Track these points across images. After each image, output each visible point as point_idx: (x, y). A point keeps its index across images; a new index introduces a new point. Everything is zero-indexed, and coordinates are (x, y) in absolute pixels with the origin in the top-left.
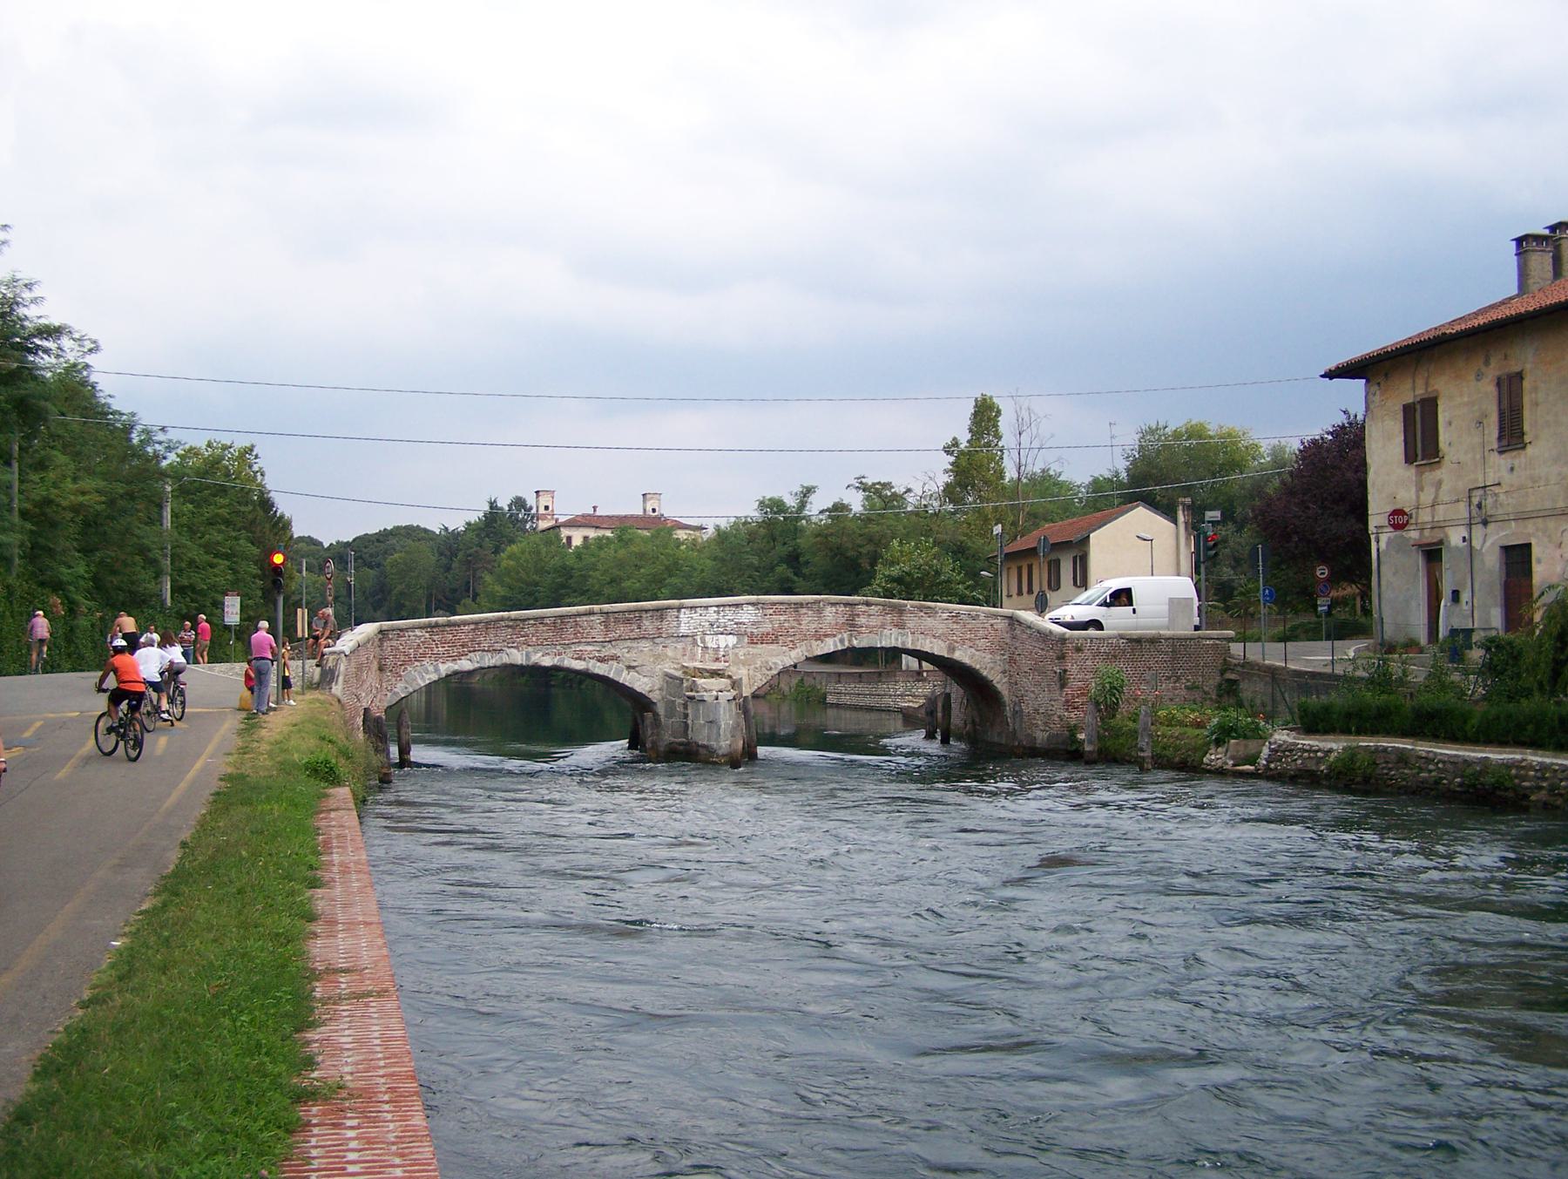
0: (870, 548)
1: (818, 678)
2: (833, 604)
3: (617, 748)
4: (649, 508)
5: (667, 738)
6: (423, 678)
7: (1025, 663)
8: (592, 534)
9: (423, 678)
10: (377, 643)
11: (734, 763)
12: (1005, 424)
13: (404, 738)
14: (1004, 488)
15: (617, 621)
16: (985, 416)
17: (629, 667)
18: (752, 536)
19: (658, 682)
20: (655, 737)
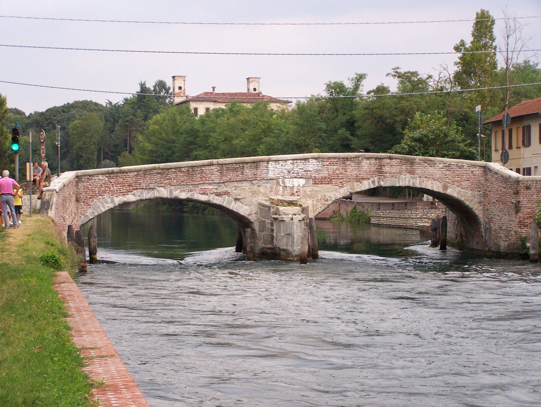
0: (402, 117)
1: (366, 206)
2: (368, 158)
3: (227, 252)
4: (251, 88)
5: (260, 245)
6: (104, 206)
7: (493, 197)
8: (212, 106)
9: (104, 206)
10: (74, 184)
11: (303, 260)
12: (498, 30)
13: (93, 244)
14: (496, 75)
15: (228, 169)
16: (483, 25)
17: (236, 199)
18: (322, 109)
19: (254, 209)
20: (251, 244)
